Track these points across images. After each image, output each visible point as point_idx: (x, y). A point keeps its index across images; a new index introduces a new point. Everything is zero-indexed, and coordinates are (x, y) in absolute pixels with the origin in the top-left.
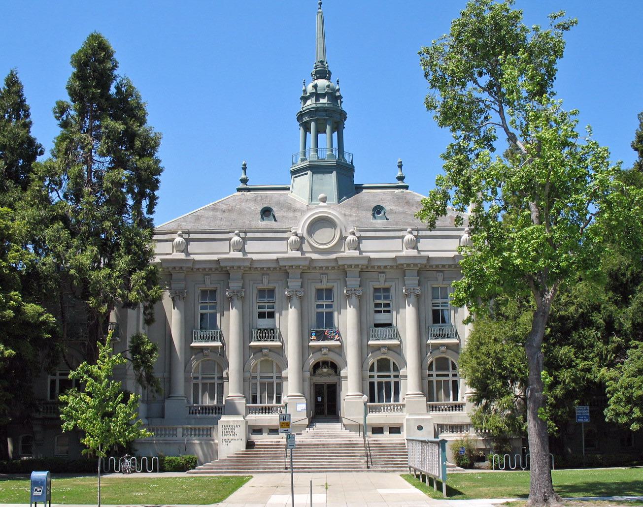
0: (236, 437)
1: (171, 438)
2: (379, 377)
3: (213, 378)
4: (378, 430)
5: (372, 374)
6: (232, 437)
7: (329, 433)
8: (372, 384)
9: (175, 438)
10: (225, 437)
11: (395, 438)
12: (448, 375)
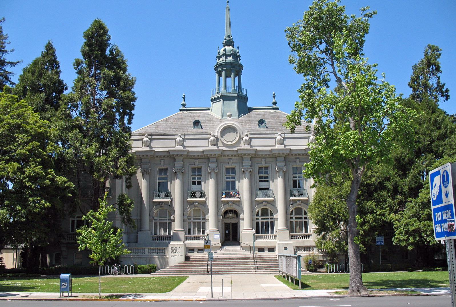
0: (179, 254)
1: (141, 254)
2: (262, 219)
3: (166, 220)
4: (261, 250)
5: (258, 217)
6: (177, 254)
7: (233, 251)
8: (258, 223)
9: (143, 254)
10: (172, 254)
11: (271, 255)
12: (302, 218)
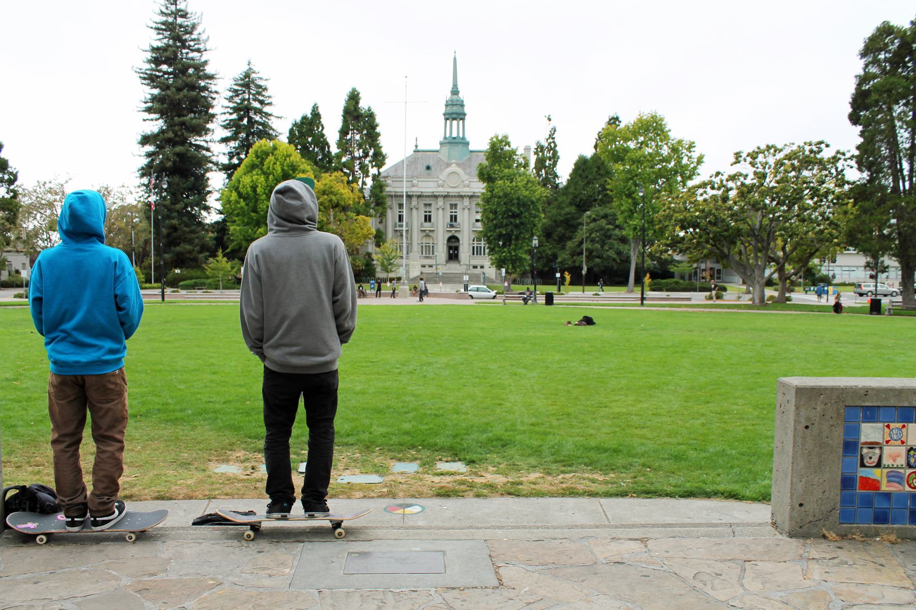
4: (475, 267)
7: (454, 268)
